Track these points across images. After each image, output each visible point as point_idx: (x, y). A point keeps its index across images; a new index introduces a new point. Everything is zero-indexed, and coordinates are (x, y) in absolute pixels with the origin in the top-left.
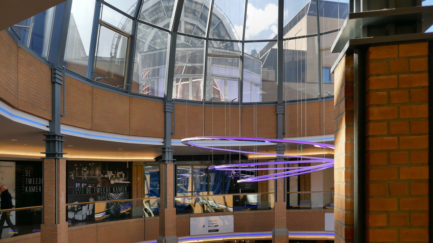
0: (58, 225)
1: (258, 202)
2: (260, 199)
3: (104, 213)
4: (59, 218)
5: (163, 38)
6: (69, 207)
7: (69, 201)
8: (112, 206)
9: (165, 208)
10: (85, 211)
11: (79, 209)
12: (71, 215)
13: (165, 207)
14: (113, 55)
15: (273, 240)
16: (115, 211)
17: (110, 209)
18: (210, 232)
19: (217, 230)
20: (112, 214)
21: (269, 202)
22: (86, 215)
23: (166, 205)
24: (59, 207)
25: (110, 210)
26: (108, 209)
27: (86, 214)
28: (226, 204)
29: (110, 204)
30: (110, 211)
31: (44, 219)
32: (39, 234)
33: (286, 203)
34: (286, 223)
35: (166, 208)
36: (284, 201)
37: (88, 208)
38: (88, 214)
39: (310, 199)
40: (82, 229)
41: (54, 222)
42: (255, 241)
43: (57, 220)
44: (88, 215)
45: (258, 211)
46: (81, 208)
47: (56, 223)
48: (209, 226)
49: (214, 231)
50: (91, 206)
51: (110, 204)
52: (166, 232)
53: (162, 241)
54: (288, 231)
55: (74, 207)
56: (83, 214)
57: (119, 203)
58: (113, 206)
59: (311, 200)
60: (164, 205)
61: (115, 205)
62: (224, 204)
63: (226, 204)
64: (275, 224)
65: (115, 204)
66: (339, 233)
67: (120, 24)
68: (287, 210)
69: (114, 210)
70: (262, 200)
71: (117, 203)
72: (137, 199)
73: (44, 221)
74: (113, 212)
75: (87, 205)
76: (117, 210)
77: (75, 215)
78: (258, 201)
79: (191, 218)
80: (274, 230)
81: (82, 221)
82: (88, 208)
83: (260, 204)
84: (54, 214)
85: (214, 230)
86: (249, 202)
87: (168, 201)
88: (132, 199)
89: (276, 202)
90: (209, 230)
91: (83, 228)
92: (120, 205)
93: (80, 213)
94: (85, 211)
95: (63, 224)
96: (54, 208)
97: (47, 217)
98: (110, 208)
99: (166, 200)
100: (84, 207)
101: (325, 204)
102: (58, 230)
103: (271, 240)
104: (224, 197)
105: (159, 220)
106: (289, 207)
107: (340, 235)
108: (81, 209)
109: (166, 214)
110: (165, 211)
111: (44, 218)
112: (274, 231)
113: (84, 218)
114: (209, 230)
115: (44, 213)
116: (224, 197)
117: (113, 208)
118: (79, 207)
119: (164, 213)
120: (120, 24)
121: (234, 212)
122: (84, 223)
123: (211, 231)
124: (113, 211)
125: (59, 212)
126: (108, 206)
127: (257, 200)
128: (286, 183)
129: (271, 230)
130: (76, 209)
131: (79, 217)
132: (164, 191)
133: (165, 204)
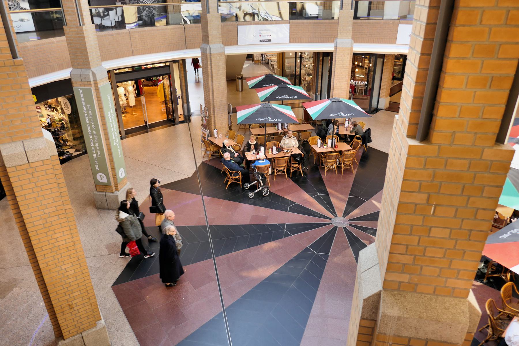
0: (84, 27)
3: (136, 24)
6: (94, 11)
7: (91, 3)
10: (113, 17)
11: (106, 14)
12: (97, 21)
15: (334, 53)
17: (142, 15)
19: (270, 40)
21: (333, 11)
22: (115, 21)
23: (209, 9)
24: (80, 7)
25: (143, 16)
30: (142, 17)
32: (63, 38)
33: (353, 11)
34: (351, 34)
35: (209, 13)
36: (351, 9)
37: (116, 14)
38: (117, 20)
39: (383, 9)
40: (112, 35)
41: (78, 23)
42: (314, 53)
43: (82, 22)
44: (117, 21)
45: (319, 20)
47: (80, 25)
48: (260, 36)
50: (119, 10)
52: (210, 39)
53: (206, 49)
54: (353, 42)
55: (99, 12)
56: (111, 20)
57: (152, 9)
58: (145, 12)
59: (384, 10)
60: (206, 10)
62: (278, 15)
64: (339, 34)
66: (417, 33)
67: (87, 312)
68: (354, 20)
69: (147, 16)
70: (324, 8)
71: (149, 8)
72: (174, 3)
73: (67, 22)
74: (146, 19)
75: (115, 10)
76: (150, 16)
77: (101, 20)
78: (319, 12)
79: (238, 26)
81: (112, 28)
82: (116, 14)
83: (322, 16)
84: (77, 15)
85: (266, 40)
87: (210, 5)
88: (167, 3)
89: (342, 9)
90: (260, 40)
92: (154, 10)
94: (113, 17)
95: (89, 28)
97: (69, 18)
99: (208, 4)
100: (110, 12)
101: (400, 15)
102: (85, 32)
103: (332, 53)
104: (278, 4)
106: (356, 17)
108: (108, 15)
110: (208, 17)
111: (65, 19)
112: (337, 42)
113: (114, 24)
114: (260, 40)
116: (278, 4)
117: (145, 14)
118: (106, 12)
120: (87, 312)
125: (81, 12)
126: (139, 11)
129: (333, 42)
130: (102, 15)
131: (106, 22)
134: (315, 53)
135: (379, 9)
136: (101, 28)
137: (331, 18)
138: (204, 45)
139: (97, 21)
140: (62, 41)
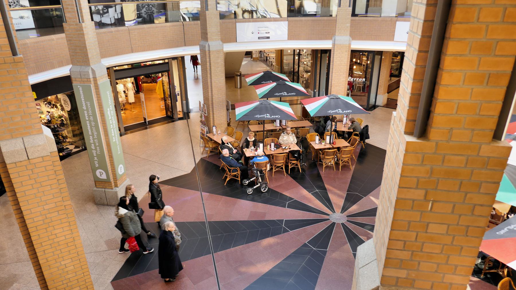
0: (83, 24)
1: (318, 11)
2: (319, 7)
4: (82, 16)
5: (228, 166)
6: (93, 8)
8: (143, 9)
9: (206, 11)
10: (112, 15)
11: (105, 11)
12: (97, 18)
13: (206, 10)
14: (169, 113)
15: (332, 51)
16: (148, 14)
17: (141, 12)
18: (260, 39)
19: (268, 38)
20: (144, 18)
21: (331, 9)
23: (207, 6)
24: (80, 5)
25: (142, 13)
26: (139, 12)
27: (114, 17)
28: (279, 13)
29: (141, 7)
30: (141, 14)
31: (66, 17)
32: (63, 35)
33: (351, 8)
34: (349, 31)
35: (208, 10)
36: (349, 6)
37: (116, 11)
38: (116, 17)
39: (381, 7)
40: (112, 32)
41: (78, 20)
44: (117, 19)
46: (106, 10)
47: (80, 22)
48: (259, 33)
49: (264, 38)
50: (118, 8)
51: (141, 7)
52: (209, 36)
53: (205, 46)
54: (351, 39)
55: (98, 9)
57: (151, 6)
58: (144, 9)
61: (147, 8)
62: (276, 12)
63: (279, 13)
64: (337, 31)
65: (146, 6)
68: (352, 17)
74: (146, 16)
76: (150, 13)
77: (101, 18)
78: (317, 10)
80: (335, 38)
81: (111, 25)
82: (116, 11)
83: (320, 13)
86: (306, 11)
89: (340, 7)
90: (259, 37)
91: (112, 31)
92: (153, 8)
93: (106, 16)
94: (112, 15)
95: (88, 26)
96: (75, 6)
97: (69, 15)
98: (141, 11)
100: (110, 10)
105: (200, 25)
106: (354, 14)
107: (411, 60)
108: (108, 12)
109: (207, 17)
112: (335, 40)
113: (113, 21)
114: (259, 37)
115: (64, 11)
118: (105, 10)
119: (205, 16)
121: (288, 18)
122: (113, 27)
123: (261, 38)
124: (145, 14)
125: (81, 9)
126: (138, 8)
127: (316, 9)
128: (352, 3)
129: (331, 39)
130: (101, 12)
131: (106, 20)
132: (205, 6)
133: (205, 6)
134: (314, 50)
135: (376, 7)
136: (100, 25)
137: (329, 15)
138: (202, 43)
139: (97, 18)
140: (62, 38)
